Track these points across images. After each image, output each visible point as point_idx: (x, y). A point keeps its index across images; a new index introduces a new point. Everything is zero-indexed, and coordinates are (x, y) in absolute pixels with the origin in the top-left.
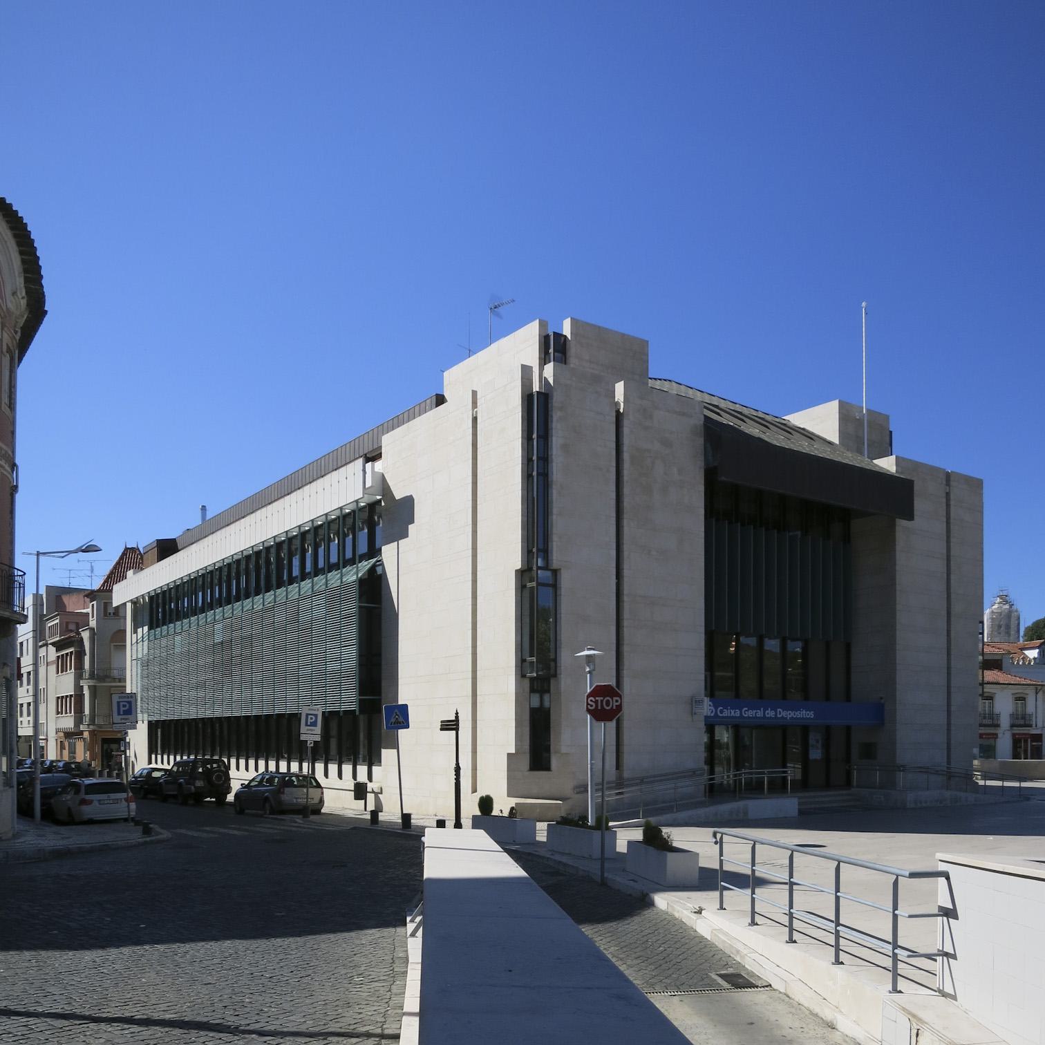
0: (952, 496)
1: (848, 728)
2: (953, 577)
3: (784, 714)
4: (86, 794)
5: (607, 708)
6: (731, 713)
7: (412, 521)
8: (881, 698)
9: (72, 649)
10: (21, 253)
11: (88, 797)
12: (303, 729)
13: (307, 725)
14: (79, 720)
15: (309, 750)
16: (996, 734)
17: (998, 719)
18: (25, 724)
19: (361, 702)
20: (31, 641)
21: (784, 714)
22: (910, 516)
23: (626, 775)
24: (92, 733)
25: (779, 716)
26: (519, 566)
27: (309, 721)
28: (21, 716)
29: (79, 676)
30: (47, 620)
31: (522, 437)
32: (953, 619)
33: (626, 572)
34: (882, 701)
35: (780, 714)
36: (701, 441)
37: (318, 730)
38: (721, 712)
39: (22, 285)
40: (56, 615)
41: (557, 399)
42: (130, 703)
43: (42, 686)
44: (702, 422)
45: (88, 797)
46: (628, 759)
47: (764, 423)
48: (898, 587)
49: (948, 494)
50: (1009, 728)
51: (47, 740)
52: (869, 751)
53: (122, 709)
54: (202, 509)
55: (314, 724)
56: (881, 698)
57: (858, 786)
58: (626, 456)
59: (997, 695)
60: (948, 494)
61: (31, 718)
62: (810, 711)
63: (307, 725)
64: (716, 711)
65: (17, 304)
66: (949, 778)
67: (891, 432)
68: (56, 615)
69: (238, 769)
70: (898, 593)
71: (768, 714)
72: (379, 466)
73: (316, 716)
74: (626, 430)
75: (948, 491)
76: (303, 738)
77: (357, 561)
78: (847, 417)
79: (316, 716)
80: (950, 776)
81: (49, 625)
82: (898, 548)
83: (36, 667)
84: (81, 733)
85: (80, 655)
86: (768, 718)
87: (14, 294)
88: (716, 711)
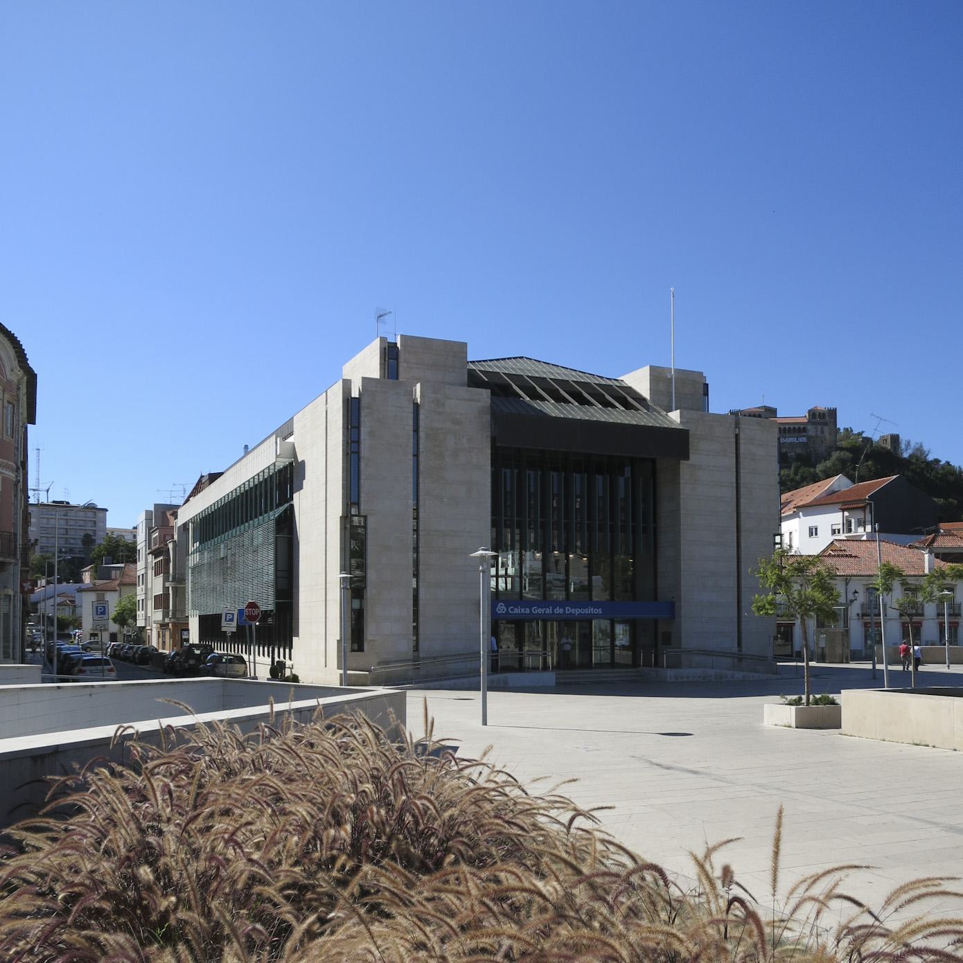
0: (742, 436)
1: (656, 621)
2: (742, 501)
3: (573, 611)
4: (83, 666)
5: (499, 612)
7: (304, 479)
8: (673, 597)
9: (161, 558)
10: (14, 348)
11: (83, 668)
12: (224, 623)
13: (226, 621)
14: (165, 615)
15: (229, 638)
16: (957, 623)
17: (960, 609)
18: (141, 616)
19: (277, 605)
20: (144, 548)
21: (573, 611)
22: (687, 458)
23: (422, 655)
24: (174, 624)
25: (567, 612)
26: (341, 515)
27: (228, 618)
28: (139, 610)
29: (166, 580)
30: (153, 532)
31: (343, 428)
32: (743, 534)
33: (743, 545)
34: (674, 599)
35: (568, 611)
36: (488, 417)
37: (234, 624)
38: (512, 610)
39: (17, 365)
40: (156, 530)
41: (363, 403)
42: (104, 607)
43: (149, 586)
44: (489, 405)
45: (83, 668)
46: (423, 645)
47: (581, 392)
48: (682, 512)
49: (737, 436)
50: (898, 618)
51: (151, 629)
52: (667, 639)
53: (99, 611)
54: (245, 448)
55: (232, 620)
56: (673, 597)
57: (643, 666)
58: (422, 434)
59: (958, 587)
60: (737, 436)
61: (143, 612)
62: (598, 609)
63: (226, 621)
64: (508, 610)
65: (14, 374)
66: (740, 660)
67: (706, 386)
68: (156, 530)
69: (259, 655)
70: (682, 516)
72: (291, 440)
73: (233, 614)
74: (422, 417)
75: (737, 432)
76: (223, 629)
77: (274, 507)
78: (657, 376)
79: (233, 614)
80: (740, 658)
81: (154, 536)
82: (682, 481)
83: (417, 523)
84: (168, 624)
85: (167, 561)
86: (557, 614)
87: (12, 370)
88: (508, 610)
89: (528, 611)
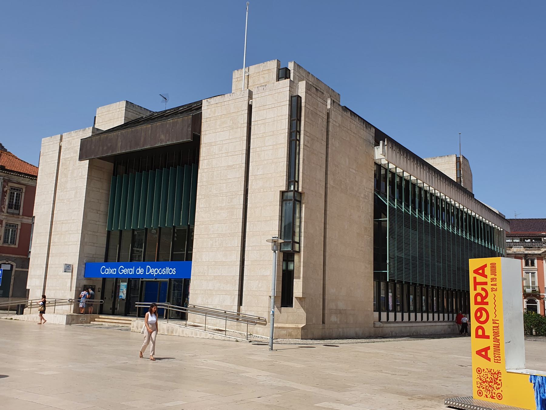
6: (110, 271)
49: (250, 107)
60: (250, 107)
71: (138, 271)
89: (140, 271)
